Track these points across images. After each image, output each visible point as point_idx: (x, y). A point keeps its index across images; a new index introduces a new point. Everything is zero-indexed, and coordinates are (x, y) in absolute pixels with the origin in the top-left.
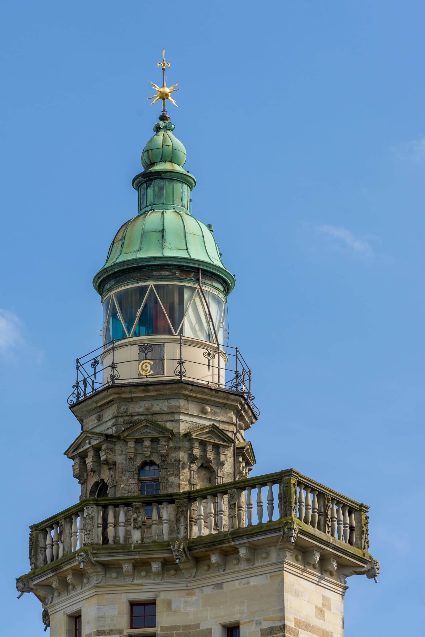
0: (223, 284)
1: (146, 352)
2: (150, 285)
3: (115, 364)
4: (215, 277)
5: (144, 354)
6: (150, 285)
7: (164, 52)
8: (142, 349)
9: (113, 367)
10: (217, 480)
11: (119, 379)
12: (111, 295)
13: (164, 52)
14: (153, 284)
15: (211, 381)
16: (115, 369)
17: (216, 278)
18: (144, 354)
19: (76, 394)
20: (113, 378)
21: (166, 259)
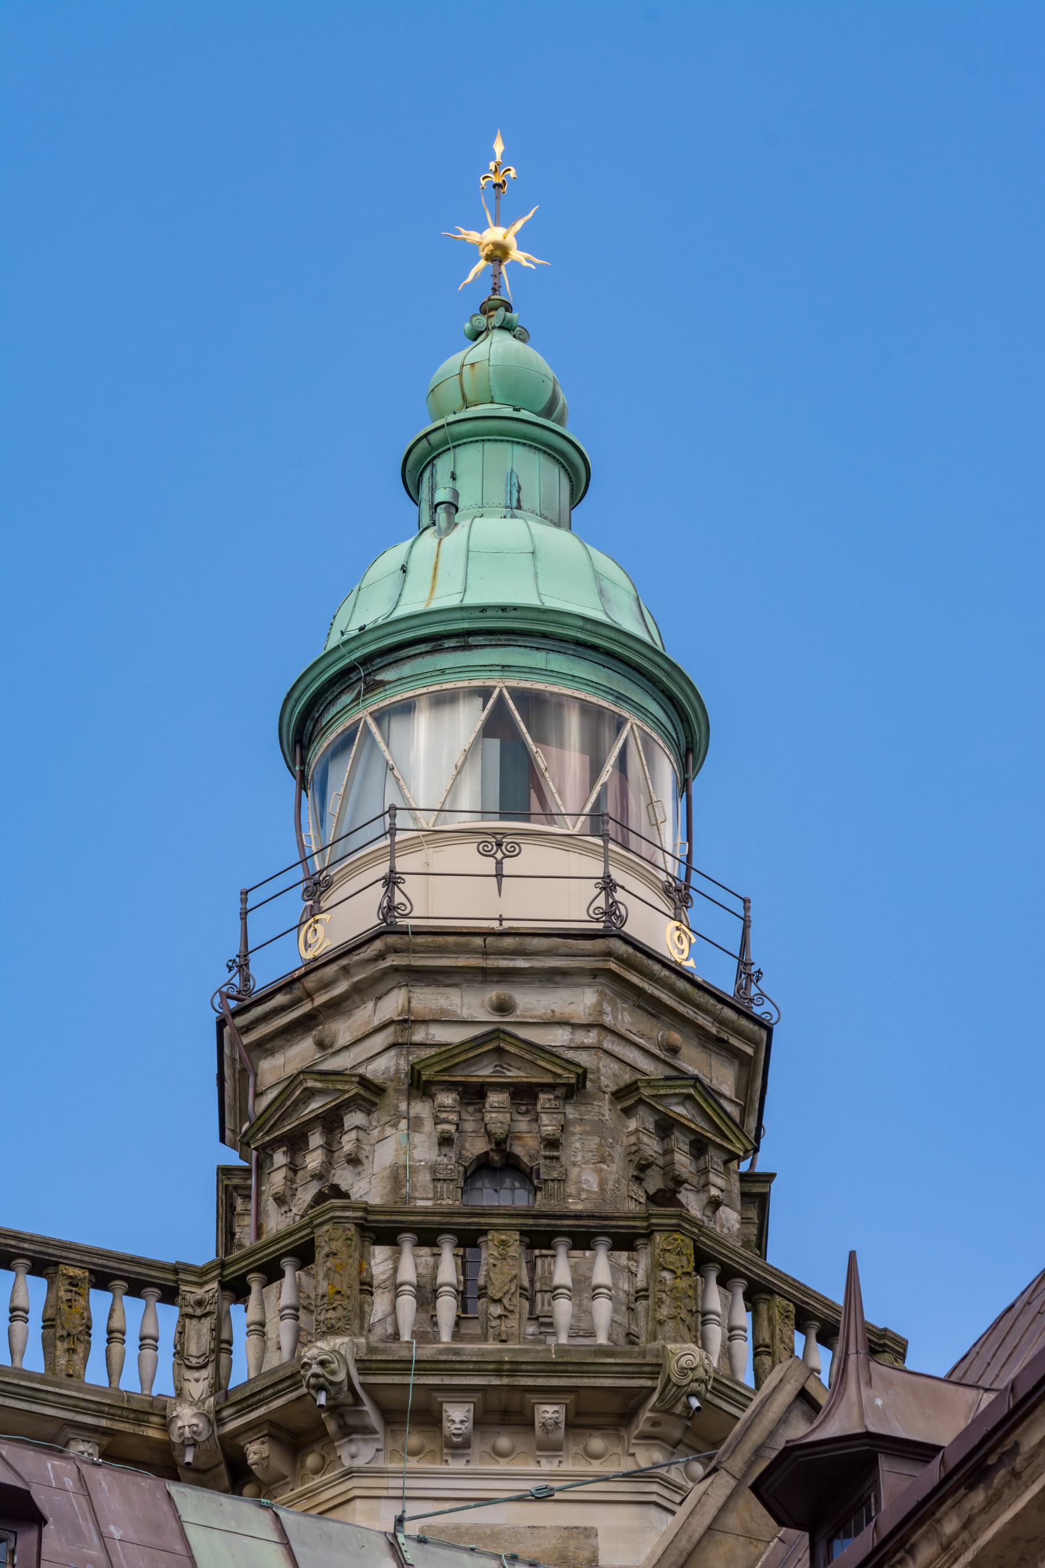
0: (327, 701)
1: (499, 855)
2: (495, 687)
3: (397, 873)
4: (318, 711)
5: (492, 861)
6: (495, 687)
7: (460, 288)
8: (486, 848)
9: (392, 880)
10: (712, 1020)
11: (410, 915)
12: (361, 718)
13: (460, 288)
14: (513, 683)
15: (671, 852)
16: (398, 887)
17: (322, 709)
18: (492, 861)
19: (238, 986)
20: (389, 909)
21: (550, 617)
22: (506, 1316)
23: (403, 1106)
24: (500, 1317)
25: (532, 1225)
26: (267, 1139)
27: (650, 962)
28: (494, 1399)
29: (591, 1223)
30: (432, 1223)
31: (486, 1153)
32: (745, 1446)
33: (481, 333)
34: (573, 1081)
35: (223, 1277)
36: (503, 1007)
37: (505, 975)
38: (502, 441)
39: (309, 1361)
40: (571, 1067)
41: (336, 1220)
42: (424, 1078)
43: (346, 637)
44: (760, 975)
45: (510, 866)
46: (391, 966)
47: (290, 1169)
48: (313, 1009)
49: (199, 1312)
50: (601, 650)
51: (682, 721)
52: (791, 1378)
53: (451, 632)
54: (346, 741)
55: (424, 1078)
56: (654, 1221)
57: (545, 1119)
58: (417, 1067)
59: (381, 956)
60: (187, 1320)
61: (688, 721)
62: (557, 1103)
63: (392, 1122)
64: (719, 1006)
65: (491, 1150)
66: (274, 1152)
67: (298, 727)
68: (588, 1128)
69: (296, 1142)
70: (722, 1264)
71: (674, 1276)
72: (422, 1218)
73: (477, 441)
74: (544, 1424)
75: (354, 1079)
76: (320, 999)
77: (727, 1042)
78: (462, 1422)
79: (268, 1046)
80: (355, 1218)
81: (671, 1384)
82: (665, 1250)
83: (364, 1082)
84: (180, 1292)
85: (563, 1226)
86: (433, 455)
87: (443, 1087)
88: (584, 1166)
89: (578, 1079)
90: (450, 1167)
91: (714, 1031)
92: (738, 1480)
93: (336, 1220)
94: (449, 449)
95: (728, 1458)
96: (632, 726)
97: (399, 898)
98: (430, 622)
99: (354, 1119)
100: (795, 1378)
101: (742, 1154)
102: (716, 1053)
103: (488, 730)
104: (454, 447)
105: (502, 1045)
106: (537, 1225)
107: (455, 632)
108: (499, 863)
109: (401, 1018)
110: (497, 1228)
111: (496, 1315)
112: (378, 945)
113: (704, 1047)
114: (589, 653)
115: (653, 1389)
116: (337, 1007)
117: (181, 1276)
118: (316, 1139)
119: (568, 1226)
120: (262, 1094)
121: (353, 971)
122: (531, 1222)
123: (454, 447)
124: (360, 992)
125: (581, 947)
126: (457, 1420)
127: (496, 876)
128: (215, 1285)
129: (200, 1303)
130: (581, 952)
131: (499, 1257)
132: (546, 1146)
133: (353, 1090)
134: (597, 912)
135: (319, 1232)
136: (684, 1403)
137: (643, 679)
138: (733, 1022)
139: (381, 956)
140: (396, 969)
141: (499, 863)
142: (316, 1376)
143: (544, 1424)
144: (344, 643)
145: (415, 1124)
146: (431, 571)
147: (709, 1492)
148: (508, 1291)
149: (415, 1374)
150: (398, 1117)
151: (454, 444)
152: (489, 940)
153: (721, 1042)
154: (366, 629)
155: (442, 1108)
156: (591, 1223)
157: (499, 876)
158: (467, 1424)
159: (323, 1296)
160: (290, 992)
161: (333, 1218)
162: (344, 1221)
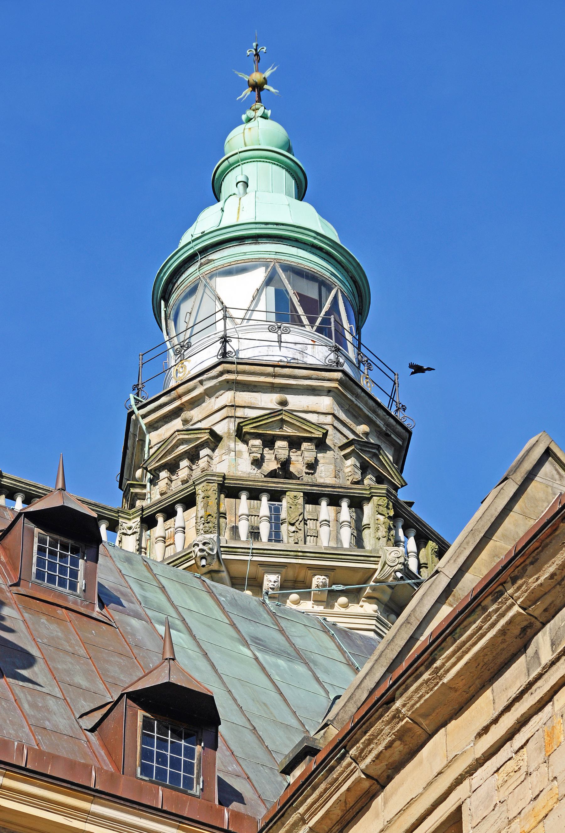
18: (276, 335)
20: (224, 354)
22: (297, 532)
23: (232, 445)
24: (294, 532)
25: (310, 490)
26: (157, 464)
27: (356, 387)
28: (291, 574)
29: (340, 490)
30: (258, 485)
31: (275, 470)
32: (521, 470)
33: (252, 119)
34: (321, 436)
35: (143, 515)
36: (284, 403)
37: (283, 389)
38: (266, 162)
39: (198, 543)
40: (320, 429)
41: (208, 481)
42: (244, 430)
43: (193, 238)
44: (404, 407)
45: (284, 337)
46: (225, 379)
47: (169, 479)
48: (182, 404)
49: (130, 532)
50: (324, 251)
51: (359, 296)
52: (542, 441)
53: (249, 235)
54: (193, 291)
55: (244, 430)
56: (372, 491)
57: (306, 454)
58: (241, 425)
59: (221, 374)
60: (123, 536)
61: (361, 296)
62: (312, 447)
63: (226, 453)
64: (388, 417)
65: (278, 468)
66: (160, 472)
67: (164, 289)
68: (327, 461)
69: (173, 467)
70: (405, 519)
71: (385, 517)
72: (252, 483)
73: (254, 161)
74: (317, 585)
75: (207, 431)
76: (185, 399)
77: (390, 436)
78: (275, 582)
79: (156, 425)
80: (218, 481)
81: (387, 565)
82: (379, 505)
83: (212, 433)
84: (120, 522)
85: (325, 491)
86: (230, 169)
87: (254, 436)
88: (326, 479)
89: (323, 435)
90: (256, 475)
91: (384, 429)
92: (552, 441)
93: (208, 481)
94: (239, 165)
95: (513, 474)
96: (337, 291)
97: (228, 349)
98: (239, 229)
99: (204, 452)
100: (544, 441)
101: (400, 486)
102: (384, 442)
103: (268, 282)
104: (242, 164)
105: (284, 418)
106: (312, 490)
107: (251, 235)
108: (280, 336)
109: (231, 404)
110: (291, 490)
111: (292, 531)
112: (220, 368)
113: (378, 437)
114: (318, 252)
115: (376, 570)
116: (196, 402)
117: (120, 514)
118: (184, 463)
119: (328, 491)
120: (152, 448)
121: (204, 383)
122: (309, 488)
123: (242, 164)
124: (210, 393)
125: (323, 375)
126: (273, 581)
127: (278, 342)
128: (138, 519)
129: (130, 528)
130: (323, 378)
131: (293, 504)
132: (307, 467)
133: (205, 436)
134: (330, 361)
135: (197, 488)
136: (394, 576)
137: (342, 269)
138: (393, 426)
139: (221, 374)
140: (227, 381)
141: (280, 336)
142: (202, 550)
143: (317, 585)
144: (193, 241)
145: (238, 454)
146: (237, 210)
147: (504, 488)
148: (298, 520)
149: (251, 556)
150: (230, 450)
151: (242, 162)
152: (276, 369)
153: (387, 435)
154: (205, 233)
155: (253, 446)
156: (340, 490)
157: (280, 342)
158: (277, 583)
159: (202, 517)
160: (169, 396)
161: (207, 480)
162: (212, 481)
